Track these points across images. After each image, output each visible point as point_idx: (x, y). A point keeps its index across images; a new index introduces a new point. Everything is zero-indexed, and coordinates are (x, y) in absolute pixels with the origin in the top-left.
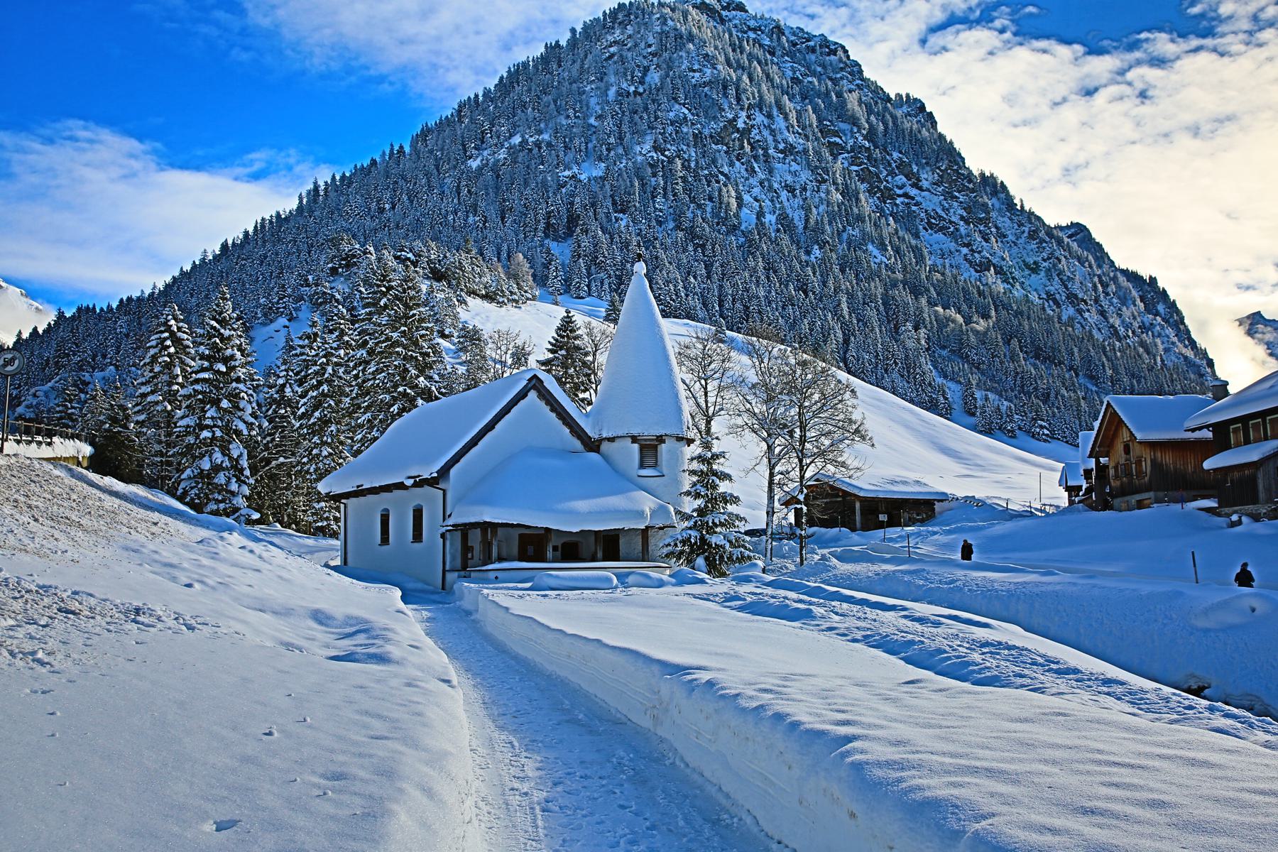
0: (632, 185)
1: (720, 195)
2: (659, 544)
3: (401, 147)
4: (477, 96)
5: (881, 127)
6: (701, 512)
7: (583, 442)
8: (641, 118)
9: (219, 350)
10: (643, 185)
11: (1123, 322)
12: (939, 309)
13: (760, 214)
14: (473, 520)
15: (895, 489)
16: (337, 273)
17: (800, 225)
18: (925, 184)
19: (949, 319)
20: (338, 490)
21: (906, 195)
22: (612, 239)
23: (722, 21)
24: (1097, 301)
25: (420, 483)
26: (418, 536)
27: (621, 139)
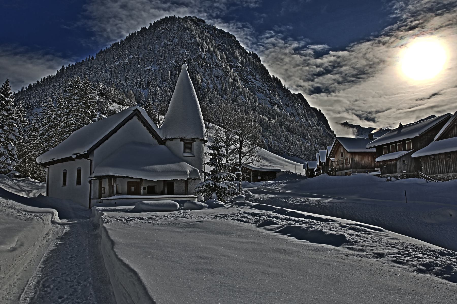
0: (168, 73)
1: (196, 78)
2: (192, 186)
3: (93, 57)
4: (118, 42)
5: (245, 61)
6: (214, 172)
7: (158, 141)
8: (172, 52)
9: (4, 106)
10: (171, 73)
11: (312, 123)
12: (261, 116)
13: (208, 84)
14: (104, 174)
15: (264, 168)
16: (66, 92)
17: (220, 89)
18: (257, 79)
19: (264, 119)
20: (44, 161)
21: (252, 82)
22: (161, 89)
23: (198, 25)
24: (305, 116)
25: (80, 157)
26: (79, 182)
27: (165, 58)
